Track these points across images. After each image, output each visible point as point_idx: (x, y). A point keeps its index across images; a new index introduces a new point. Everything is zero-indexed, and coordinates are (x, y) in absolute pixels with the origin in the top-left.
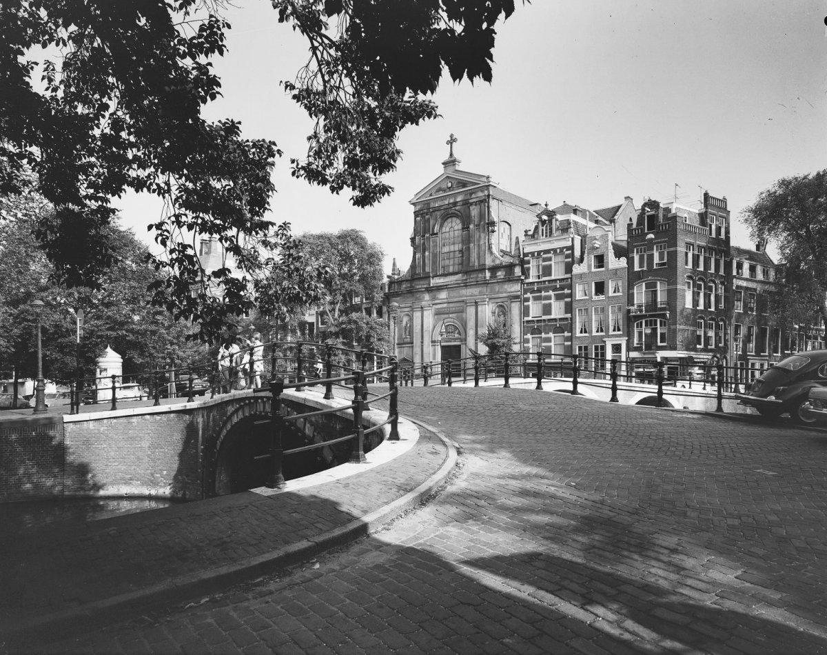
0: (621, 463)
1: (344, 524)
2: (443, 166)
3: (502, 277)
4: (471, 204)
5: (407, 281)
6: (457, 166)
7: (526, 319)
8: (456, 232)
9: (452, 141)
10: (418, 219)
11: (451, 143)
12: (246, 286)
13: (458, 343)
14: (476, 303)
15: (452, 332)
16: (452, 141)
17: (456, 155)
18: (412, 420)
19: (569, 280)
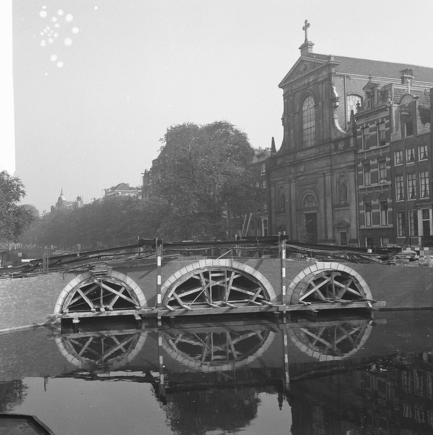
0: (178, 387)
1: (337, 336)
2: (300, 50)
3: (342, 148)
4: (319, 83)
5: (280, 157)
6: (309, 49)
7: (361, 187)
8: (311, 110)
9: (307, 26)
10: (286, 100)
11: (306, 28)
12: (113, 308)
13: (315, 212)
14: (324, 174)
15: (311, 202)
16: (307, 26)
17: (309, 39)
18: (114, 380)
19: (389, 148)
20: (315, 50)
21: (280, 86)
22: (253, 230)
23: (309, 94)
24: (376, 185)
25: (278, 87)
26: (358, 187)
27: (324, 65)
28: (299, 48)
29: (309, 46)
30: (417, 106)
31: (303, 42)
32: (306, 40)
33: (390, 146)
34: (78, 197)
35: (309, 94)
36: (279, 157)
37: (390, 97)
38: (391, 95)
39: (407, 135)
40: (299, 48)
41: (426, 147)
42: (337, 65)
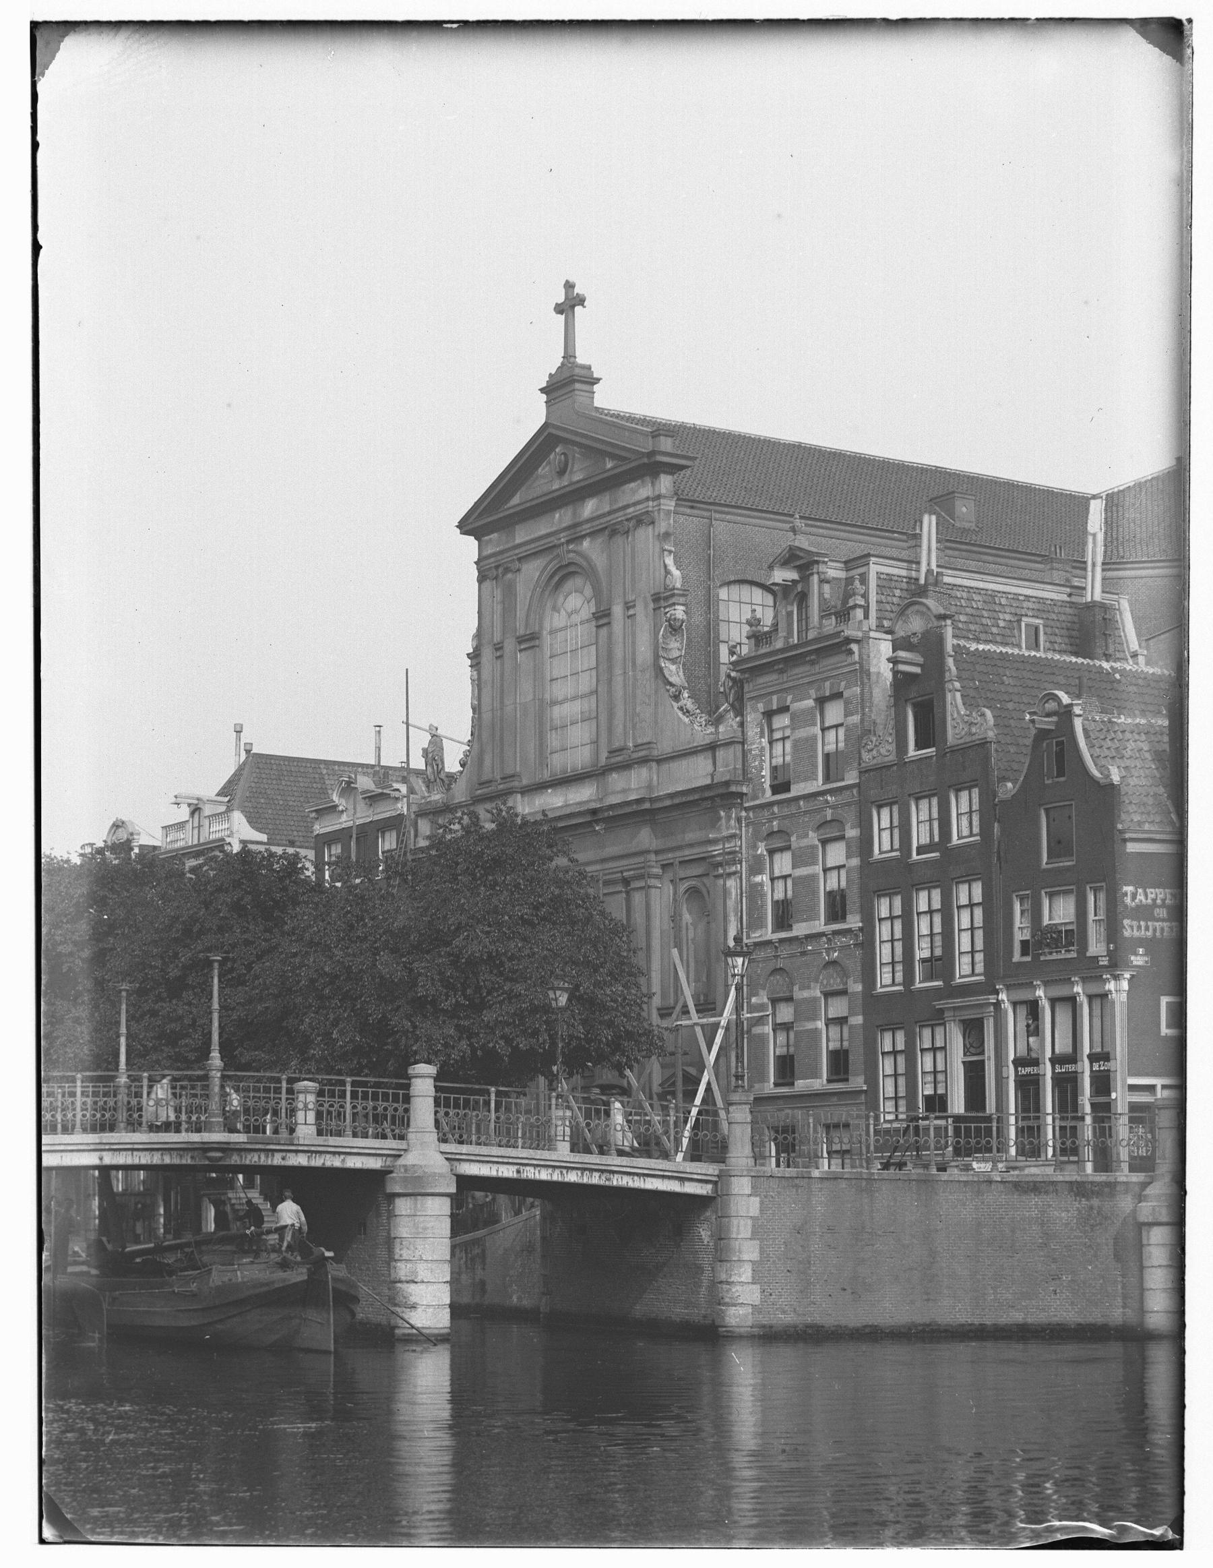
2: (544, 397)
9: (570, 304)
16: (570, 304)
20: (606, 398)
21: (467, 526)
22: (886, 1062)
23: (572, 569)
24: (783, 935)
25: (458, 531)
26: (748, 937)
27: (633, 464)
28: (542, 390)
29: (578, 386)
30: (949, 648)
31: (553, 362)
32: (569, 355)
33: (857, 785)
34: (567, 282)
35: (572, 569)
36: (523, 793)
37: (860, 606)
38: (865, 596)
39: (919, 746)
40: (542, 390)
41: (975, 792)
42: (682, 467)
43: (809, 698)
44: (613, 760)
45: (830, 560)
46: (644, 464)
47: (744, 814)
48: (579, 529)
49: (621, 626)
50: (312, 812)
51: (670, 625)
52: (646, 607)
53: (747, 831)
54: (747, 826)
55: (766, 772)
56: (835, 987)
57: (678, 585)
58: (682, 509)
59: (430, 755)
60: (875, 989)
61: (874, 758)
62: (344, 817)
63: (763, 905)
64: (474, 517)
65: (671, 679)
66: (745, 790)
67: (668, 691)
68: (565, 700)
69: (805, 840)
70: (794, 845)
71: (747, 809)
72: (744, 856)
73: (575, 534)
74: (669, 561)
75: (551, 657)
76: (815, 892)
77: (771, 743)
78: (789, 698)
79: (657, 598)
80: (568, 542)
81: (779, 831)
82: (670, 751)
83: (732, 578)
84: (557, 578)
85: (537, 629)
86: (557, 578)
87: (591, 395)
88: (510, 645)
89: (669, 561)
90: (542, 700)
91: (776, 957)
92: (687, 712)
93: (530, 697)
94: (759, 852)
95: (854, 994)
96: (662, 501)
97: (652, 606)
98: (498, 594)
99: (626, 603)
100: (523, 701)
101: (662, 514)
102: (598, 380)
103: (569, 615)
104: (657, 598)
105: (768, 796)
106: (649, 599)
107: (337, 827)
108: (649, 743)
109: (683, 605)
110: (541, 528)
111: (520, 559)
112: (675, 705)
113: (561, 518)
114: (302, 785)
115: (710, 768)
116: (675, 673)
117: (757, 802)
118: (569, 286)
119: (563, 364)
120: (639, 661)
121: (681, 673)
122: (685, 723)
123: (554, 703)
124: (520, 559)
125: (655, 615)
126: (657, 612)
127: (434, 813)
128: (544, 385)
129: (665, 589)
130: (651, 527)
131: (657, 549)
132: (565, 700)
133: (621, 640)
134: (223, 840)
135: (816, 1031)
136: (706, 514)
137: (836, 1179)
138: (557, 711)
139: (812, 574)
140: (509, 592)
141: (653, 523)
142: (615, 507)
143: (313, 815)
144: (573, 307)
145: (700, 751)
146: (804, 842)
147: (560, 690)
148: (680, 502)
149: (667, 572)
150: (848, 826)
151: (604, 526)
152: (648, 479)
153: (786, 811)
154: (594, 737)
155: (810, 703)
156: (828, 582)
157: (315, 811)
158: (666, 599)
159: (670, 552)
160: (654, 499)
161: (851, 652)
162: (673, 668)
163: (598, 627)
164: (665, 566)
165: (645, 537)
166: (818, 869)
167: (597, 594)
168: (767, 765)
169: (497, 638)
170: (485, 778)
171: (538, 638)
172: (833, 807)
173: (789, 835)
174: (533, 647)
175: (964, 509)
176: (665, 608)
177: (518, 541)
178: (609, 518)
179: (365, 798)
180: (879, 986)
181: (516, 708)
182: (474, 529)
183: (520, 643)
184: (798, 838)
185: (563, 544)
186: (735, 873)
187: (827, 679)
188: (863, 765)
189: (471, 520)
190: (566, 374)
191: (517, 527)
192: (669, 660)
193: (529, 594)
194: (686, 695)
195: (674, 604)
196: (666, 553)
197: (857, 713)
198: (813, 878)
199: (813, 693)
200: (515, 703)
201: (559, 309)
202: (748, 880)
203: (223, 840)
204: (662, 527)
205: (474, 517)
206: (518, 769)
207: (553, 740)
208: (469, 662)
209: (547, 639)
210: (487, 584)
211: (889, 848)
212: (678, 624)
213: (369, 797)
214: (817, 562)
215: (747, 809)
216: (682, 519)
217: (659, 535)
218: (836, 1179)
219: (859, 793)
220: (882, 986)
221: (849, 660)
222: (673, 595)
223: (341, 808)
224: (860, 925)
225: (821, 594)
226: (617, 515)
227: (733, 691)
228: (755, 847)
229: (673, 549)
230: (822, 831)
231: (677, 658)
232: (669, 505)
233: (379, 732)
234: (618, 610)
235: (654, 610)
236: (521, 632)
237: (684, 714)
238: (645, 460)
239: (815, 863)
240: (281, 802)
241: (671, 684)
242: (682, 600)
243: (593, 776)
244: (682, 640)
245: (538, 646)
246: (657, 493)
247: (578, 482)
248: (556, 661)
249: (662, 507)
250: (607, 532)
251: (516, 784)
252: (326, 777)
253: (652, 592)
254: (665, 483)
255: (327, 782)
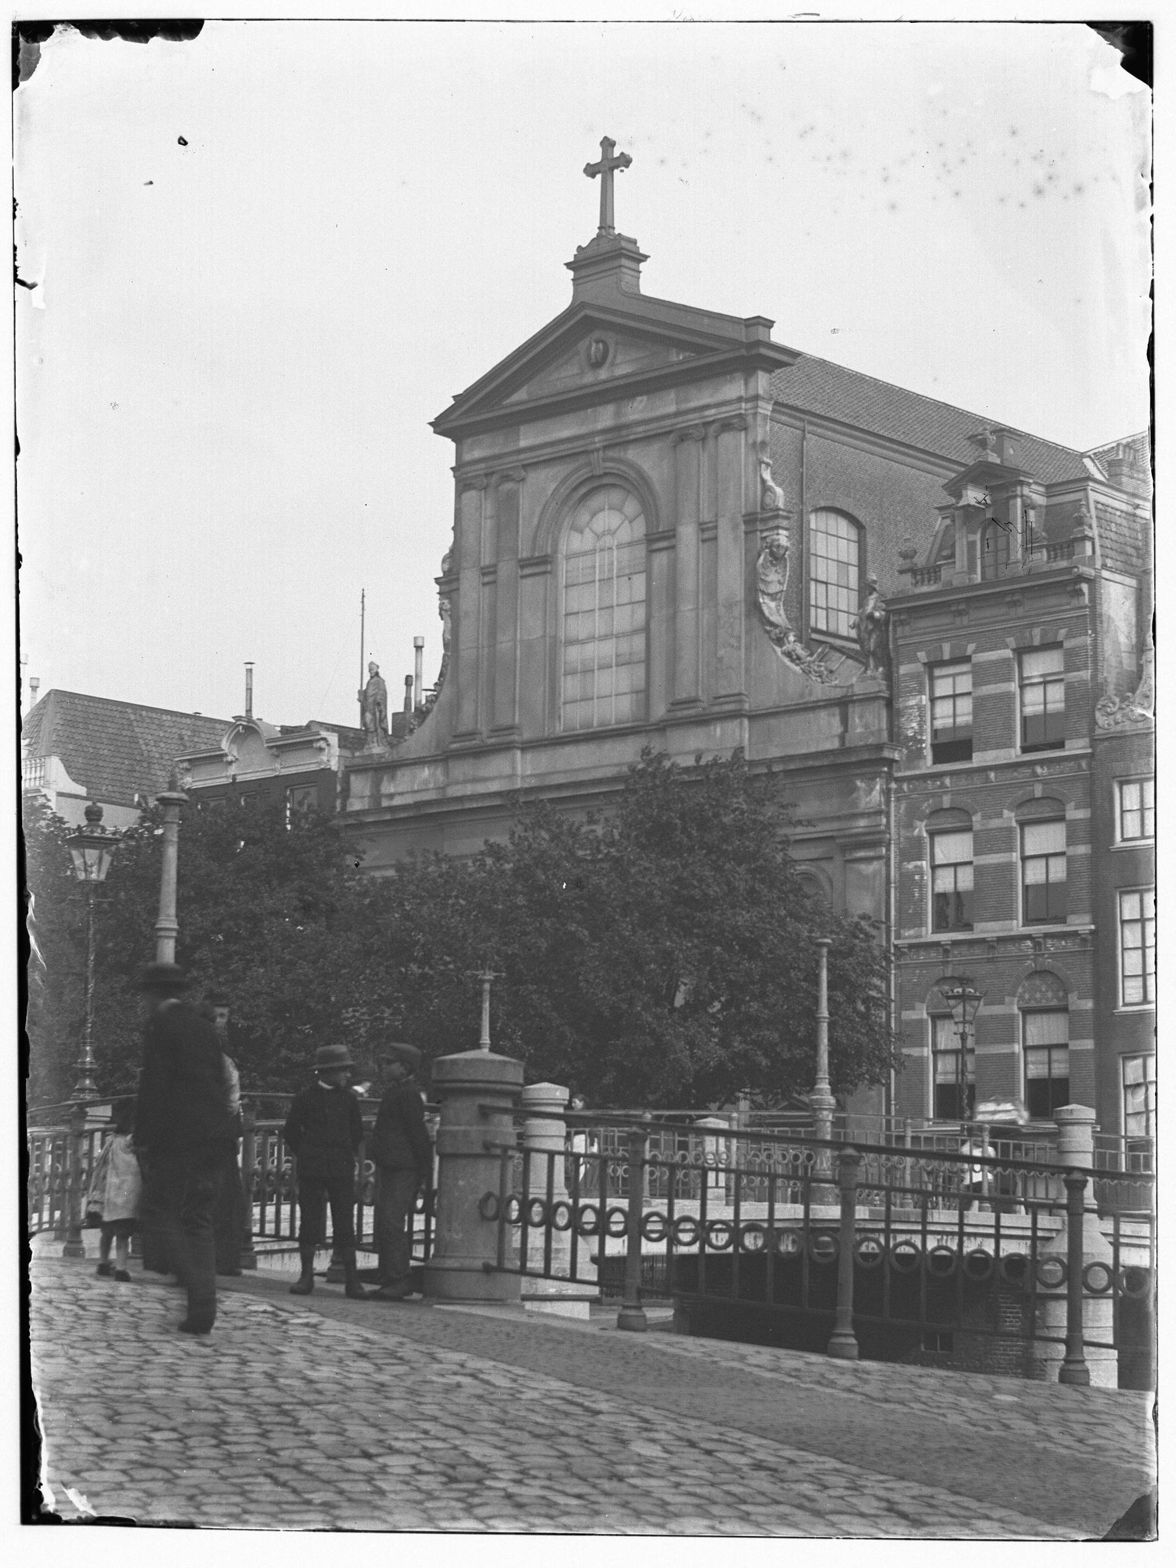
2: (571, 274)
28: (569, 265)
29: (624, 262)
31: (588, 232)
32: (606, 224)
40: (569, 265)
43: (1006, 647)
44: (679, 714)
45: (1036, 483)
46: (742, 356)
47: (893, 786)
48: (624, 433)
49: (693, 550)
50: (182, 761)
51: (772, 554)
52: (735, 527)
53: (898, 808)
54: (898, 799)
55: (927, 737)
56: (1044, 1003)
57: (781, 505)
58: (777, 416)
59: (370, 700)
60: (1115, 1007)
61: (1117, 723)
62: (232, 770)
63: (922, 899)
64: (458, 412)
65: (773, 619)
66: (897, 756)
67: (768, 632)
68: (591, 638)
69: (996, 821)
70: (977, 826)
71: (897, 780)
72: (894, 836)
73: (619, 437)
74: (767, 475)
75: (566, 587)
76: (1011, 886)
77: (933, 700)
78: (971, 647)
79: (751, 520)
80: (605, 448)
81: (952, 809)
82: (771, 704)
83: (823, 504)
84: (583, 490)
85: (549, 551)
86: (583, 490)
87: (635, 274)
88: (506, 569)
89: (767, 475)
90: (555, 638)
91: (945, 963)
92: (797, 659)
93: (540, 633)
94: (916, 832)
95: (1080, 1013)
96: (760, 403)
97: (743, 527)
98: (489, 508)
99: (700, 524)
100: (526, 638)
101: (759, 418)
102: (646, 257)
103: (598, 537)
104: (751, 520)
105: (927, 764)
106: (740, 520)
107: (313, 768)
108: (740, 694)
109: (786, 529)
110: (565, 429)
111: (525, 467)
112: (778, 650)
113: (605, 417)
114: (110, 730)
115: (838, 729)
116: (772, 609)
117: (917, 772)
118: (608, 144)
119: (598, 235)
120: (722, 594)
121: (782, 612)
122: (795, 673)
123: (570, 642)
124: (525, 467)
125: (746, 540)
126: (750, 536)
127: (376, 770)
128: (572, 259)
129: (763, 508)
130: (743, 434)
131: (752, 458)
132: (591, 638)
133: (693, 566)
134: (38, 791)
135: (921, 1062)
136: (799, 424)
137: (489, 1300)
138: (573, 654)
139: (1015, 497)
140: (508, 508)
141: (746, 429)
142: (684, 407)
143: (186, 765)
144: (612, 169)
145: (820, 707)
146: (995, 823)
147: (577, 628)
148: (778, 408)
149: (766, 489)
150: (1068, 807)
151: (667, 429)
152: (738, 375)
153: (963, 783)
154: (642, 684)
155: (1008, 653)
156: (1033, 508)
157: (189, 760)
158: (764, 520)
159: (768, 465)
160: (747, 400)
161: (1080, 593)
162: (773, 604)
163: (651, 552)
164: (763, 481)
165: (734, 444)
166: (1015, 856)
167: (649, 508)
168: (928, 727)
169: (486, 560)
170: (462, 729)
171: (551, 563)
172: (1045, 782)
173: (969, 814)
174: (545, 573)
175: (1012, 452)
176: (762, 531)
177: (523, 443)
178: (674, 421)
179: (271, 748)
180: (1121, 1003)
181: (515, 646)
182: (456, 428)
183: (522, 567)
184: (984, 817)
185: (598, 450)
186: (879, 858)
187: (1038, 624)
188: (1098, 731)
189: (453, 417)
190: (605, 247)
191: (523, 429)
192: (768, 594)
193: (539, 509)
194: (792, 638)
195: (778, 527)
196: (763, 466)
197: (1086, 668)
198: (1009, 867)
199: (1011, 641)
200: (515, 640)
201: (591, 171)
202: (899, 866)
203: (38, 791)
204: (761, 432)
205: (458, 412)
206: (517, 720)
207: (570, 687)
208: (437, 588)
209: (563, 567)
210: (472, 494)
211: (1138, 834)
212: (782, 552)
213: (277, 747)
214: (1022, 483)
215: (897, 780)
216: (777, 426)
217: (754, 443)
218: (489, 1300)
219: (1090, 767)
220: (1125, 1005)
221: (1075, 602)
222: (777, 516)
223: (230, 758)
224: (1093, 927)
225: (1026, 521)
226: (691, 416)
227: (874, 636)
228: (910, 826)
229: (771, 462)
230: (1025, 810)
231: (777, 593)
232: (766, 408)
233: (250, 670)
234: (688, 533)
235: (746, 533)
236: (524, 554)
237: (792, 661)
238: (743, 352)
239: (1011, 850)
240: (91, 750)
241: (772, 624)
242: (785, 523)
243: (641, 732)
244: (785, 571)
245: (550, 573)
246: (751, 392)
247: (605, 382)
248: (574, 592)
249: (760, 410)
250: (671, 436)
251: (516, 738)
252: (135, 724)
253: (743, 512)
254: (762, 382)
255: (137, 730)
